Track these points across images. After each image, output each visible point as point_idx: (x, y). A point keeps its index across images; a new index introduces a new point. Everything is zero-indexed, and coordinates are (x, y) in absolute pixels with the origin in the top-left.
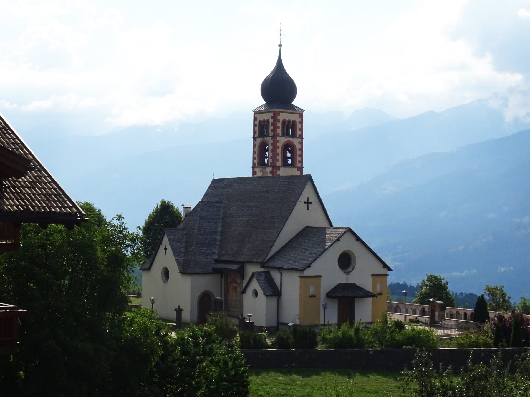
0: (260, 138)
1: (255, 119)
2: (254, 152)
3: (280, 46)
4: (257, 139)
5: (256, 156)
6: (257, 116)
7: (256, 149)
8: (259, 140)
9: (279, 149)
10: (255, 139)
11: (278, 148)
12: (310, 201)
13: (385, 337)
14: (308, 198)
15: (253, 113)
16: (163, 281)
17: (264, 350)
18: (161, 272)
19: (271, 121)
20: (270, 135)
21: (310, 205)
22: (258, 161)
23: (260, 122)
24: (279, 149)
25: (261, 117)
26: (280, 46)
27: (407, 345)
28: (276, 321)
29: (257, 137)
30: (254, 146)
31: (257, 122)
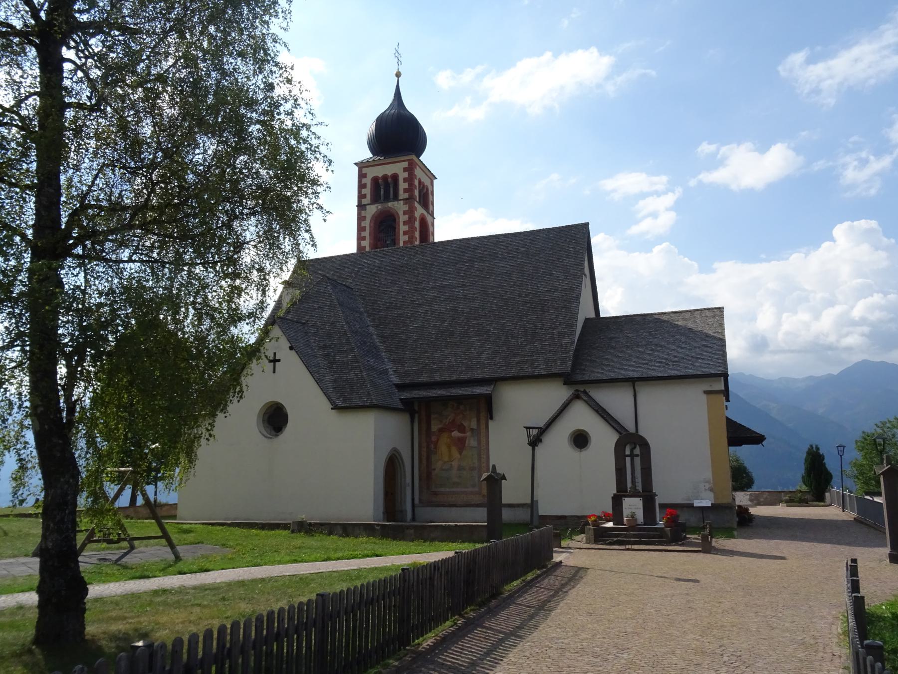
0: (376, 205)
1: (361, 176)
2: (360, 229)
3: (398, 75)
4: (368, 207)
5: (366, 234)
6: (364, 171)
7: (367, 224)
8: (372, 209)
9: (404, 222)
10: (361, 207)
11: (405, 223)
12: (277, 358)
13: (156, 632)
14: (275, 354)
15: (356, 168)
16: (260, 432)
17: (267, 632)
18: (256, 418)
19: (403, 175)
20: (401, 197)
21: (277, 363)
22: (370, 243)
23: (375, 180)
24: (404, 222)
25: (372, 172)
26: (398, 75)
27: (230, 666)
28: (845, 598)
29: (369, 204)
30: (360, 219)
31: (368, 181)
